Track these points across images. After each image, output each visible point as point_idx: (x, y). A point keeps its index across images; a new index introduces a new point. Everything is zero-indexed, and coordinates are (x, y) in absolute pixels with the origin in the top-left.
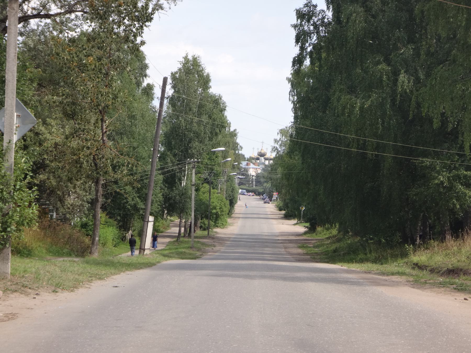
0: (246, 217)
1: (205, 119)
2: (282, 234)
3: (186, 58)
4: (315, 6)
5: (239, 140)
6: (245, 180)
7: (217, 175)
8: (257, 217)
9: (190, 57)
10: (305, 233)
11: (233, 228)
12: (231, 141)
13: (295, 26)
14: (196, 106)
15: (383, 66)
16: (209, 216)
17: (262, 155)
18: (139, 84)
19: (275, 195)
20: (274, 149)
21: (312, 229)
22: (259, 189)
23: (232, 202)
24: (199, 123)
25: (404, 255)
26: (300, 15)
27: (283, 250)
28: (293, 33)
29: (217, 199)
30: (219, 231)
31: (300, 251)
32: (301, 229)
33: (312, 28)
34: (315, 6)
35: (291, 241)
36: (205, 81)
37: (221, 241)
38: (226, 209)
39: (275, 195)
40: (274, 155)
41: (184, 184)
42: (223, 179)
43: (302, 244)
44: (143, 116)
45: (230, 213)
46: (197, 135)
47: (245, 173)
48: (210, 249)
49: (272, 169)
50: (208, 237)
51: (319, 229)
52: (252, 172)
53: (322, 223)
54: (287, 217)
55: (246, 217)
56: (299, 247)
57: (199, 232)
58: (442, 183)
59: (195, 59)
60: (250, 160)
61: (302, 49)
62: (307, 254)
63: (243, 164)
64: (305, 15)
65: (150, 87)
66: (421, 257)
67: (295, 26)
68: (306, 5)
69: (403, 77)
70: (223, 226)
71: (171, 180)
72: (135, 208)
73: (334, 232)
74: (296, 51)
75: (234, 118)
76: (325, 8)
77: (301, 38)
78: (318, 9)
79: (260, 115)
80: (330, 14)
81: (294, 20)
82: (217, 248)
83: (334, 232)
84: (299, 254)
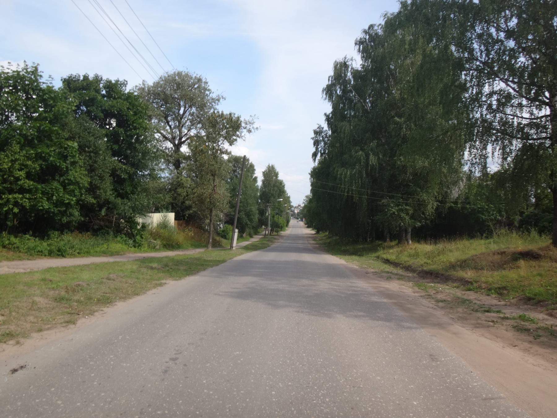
0: (294, 227)
1: (276, 188)
2: (306, 234)
3: (269, 166)
4: (323, 128)
5: (291, 199)
6: (293, 214)
7: (282, 212)
8: (298, 228)
9: (271, 165)
10: (315, 234)
11: (288, 232)
12: (287, 200)
13: (313, 138)
14: (273, 186)
15: (360, 153)
16: (277, 227)
17: (299, 206)
18: (252, 176)
19: (304, 219)
20: (304, 203)
21: (318, 232)
22: (297, 216)
23: (288, 222)
24: (273, 190)
25: (374, 249)
26: (316, 132)
27: (306, 242)
28: (312, 141)
29: (281, 220)
30: (283, 233)
31: (313, 242)
32: (313, 232)
33: (321, 138)
34: (323, 128)
35: (310, 237)
36: (276, 175)
37: (282, 237)
38: (285, 224)
39: (304, 219)
40: (304, 205)
41: (267, 214)
42: (284, 213)
43: (314, 239)
44: (250, 187)
45: (287, 226)
46: (272, 195)
47: (293, 212)
48: (276, 241)
49: (302, 211)
50: (277, 235)
51: (321, 232)
52: (296, 212)
53: (322, 230)
54: (308, 227)
55: (294, 227)
56: (313, 240)
57: (275, 233)
58: (394, 213)
59: (272, 166)
60: (295, 207)
61: (317, 149)
62: (316, 244)
63: (293, 209)
64: (317, 133)
65: (256, 178)
66: (392, 254)
67: (313, 138)
68: (318, 128)
69: (372, 157)
70: (284, 231)
71: (262, 212)
72: (247, 224)
73: (327, 233)
74: (313, 150)
75: (289, 190)
76: (327, 129)
77: (316, 143)
78: (324, 129)
79: (298, 189)
80: (330, 132)
81: (313, 135)
82: (279, 241)
83: (327, 233)
84: (313, 244)
